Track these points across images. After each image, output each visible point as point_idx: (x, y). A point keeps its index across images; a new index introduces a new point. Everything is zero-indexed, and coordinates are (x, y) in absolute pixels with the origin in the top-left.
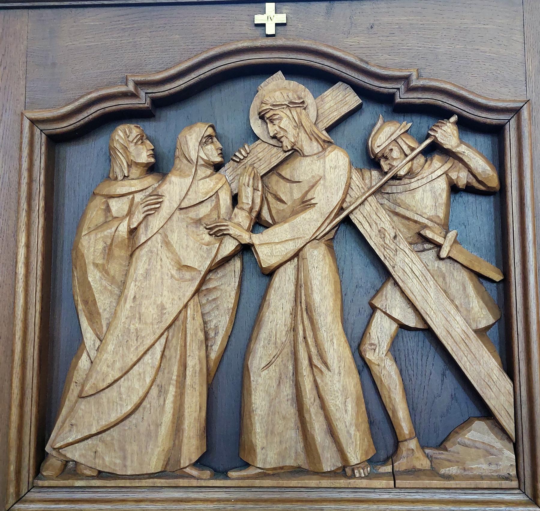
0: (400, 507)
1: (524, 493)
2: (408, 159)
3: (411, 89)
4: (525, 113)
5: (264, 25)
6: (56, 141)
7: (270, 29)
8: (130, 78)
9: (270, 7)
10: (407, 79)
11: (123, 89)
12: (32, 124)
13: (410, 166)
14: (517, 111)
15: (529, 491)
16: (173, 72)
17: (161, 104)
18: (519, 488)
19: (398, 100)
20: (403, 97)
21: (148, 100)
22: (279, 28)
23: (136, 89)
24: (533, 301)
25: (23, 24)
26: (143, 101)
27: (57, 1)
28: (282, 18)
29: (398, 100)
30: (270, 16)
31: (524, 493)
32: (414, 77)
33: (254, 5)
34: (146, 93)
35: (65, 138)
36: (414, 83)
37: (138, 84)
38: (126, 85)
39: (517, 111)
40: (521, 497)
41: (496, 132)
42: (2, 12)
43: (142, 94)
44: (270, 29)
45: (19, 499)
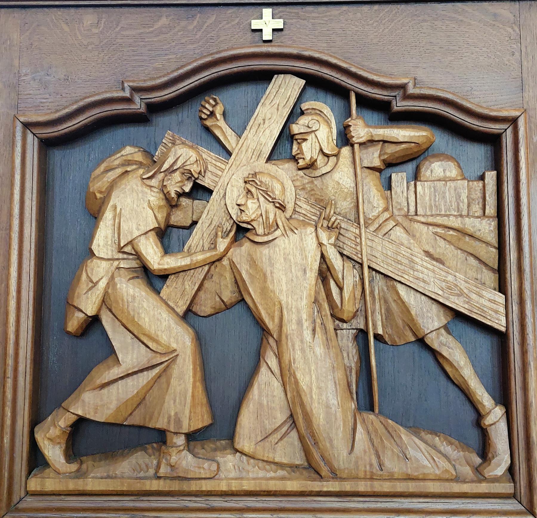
0: (5, 492)
1: (506, 129)
2: (226, 171)
3: (407, 97)
5: (261, 30)
6: (47, 145)
8: (126, 85)
9: (267, 12)
10: (403, 87)
11: (121, 94)
14: (514, 121)
15: (524, 500)
16: (376, 78)
17: (156, 108)
19: (395, 108)
20: (400, 105)
21: (143, 106)
22: (276, 33)
23: (131, 94)
24: (12, 342)
25: (9, 24)
26: (138, 105)
27: (5, 1)
28: (279, 24)
30: (267, 22)
31: (506, 129)
32: (411, 85)
34: (141, 99)
36: (411, 90)
38: (123, 89)
39: (514, 121)
40: (520, 507)
41: (493, 141)
42: (3, 10)
43: (137, 98)
44: (267, 35)
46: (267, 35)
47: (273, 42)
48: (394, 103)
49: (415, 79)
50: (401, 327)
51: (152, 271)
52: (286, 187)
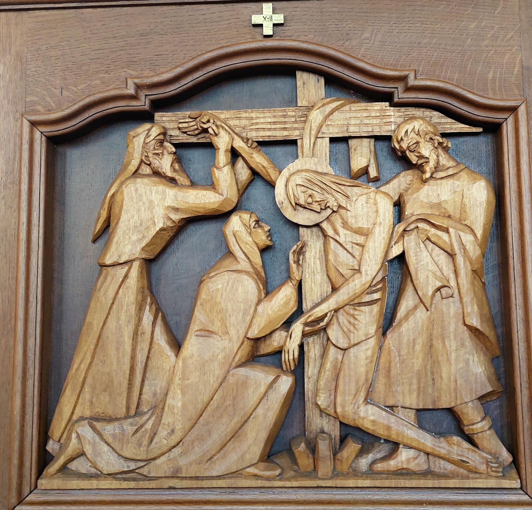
1: (506, 119)
3: (409, 89)
4: (522, 110)
5: (261, 26)
6: (56, 143)
7: (268, 30)
8: (129, 80)
9: (267, 7)
10: (403, 79)
12: (481, 256)
13: (147, 139)
16: (374, 70)
18: (521, 488)
23: (136, 92)
28: (279, 18)
29: (396, 100)
30: (267, 16)
31: (506, 119)
32: (412, 76)
33: (254, 4)
34: (146, 95)
35: (63, 141)
36: (412, 82)
37: (138, 87)
39: (513, 110)
41: (493, 130)
42: (3, 14)
45: (20, 502)
46: (268, 30)
47: (274, 36)
48: (396, 95)
49: (415, 71)
50: (451, 316)
51: (478, 177)
52: (284, 187)
